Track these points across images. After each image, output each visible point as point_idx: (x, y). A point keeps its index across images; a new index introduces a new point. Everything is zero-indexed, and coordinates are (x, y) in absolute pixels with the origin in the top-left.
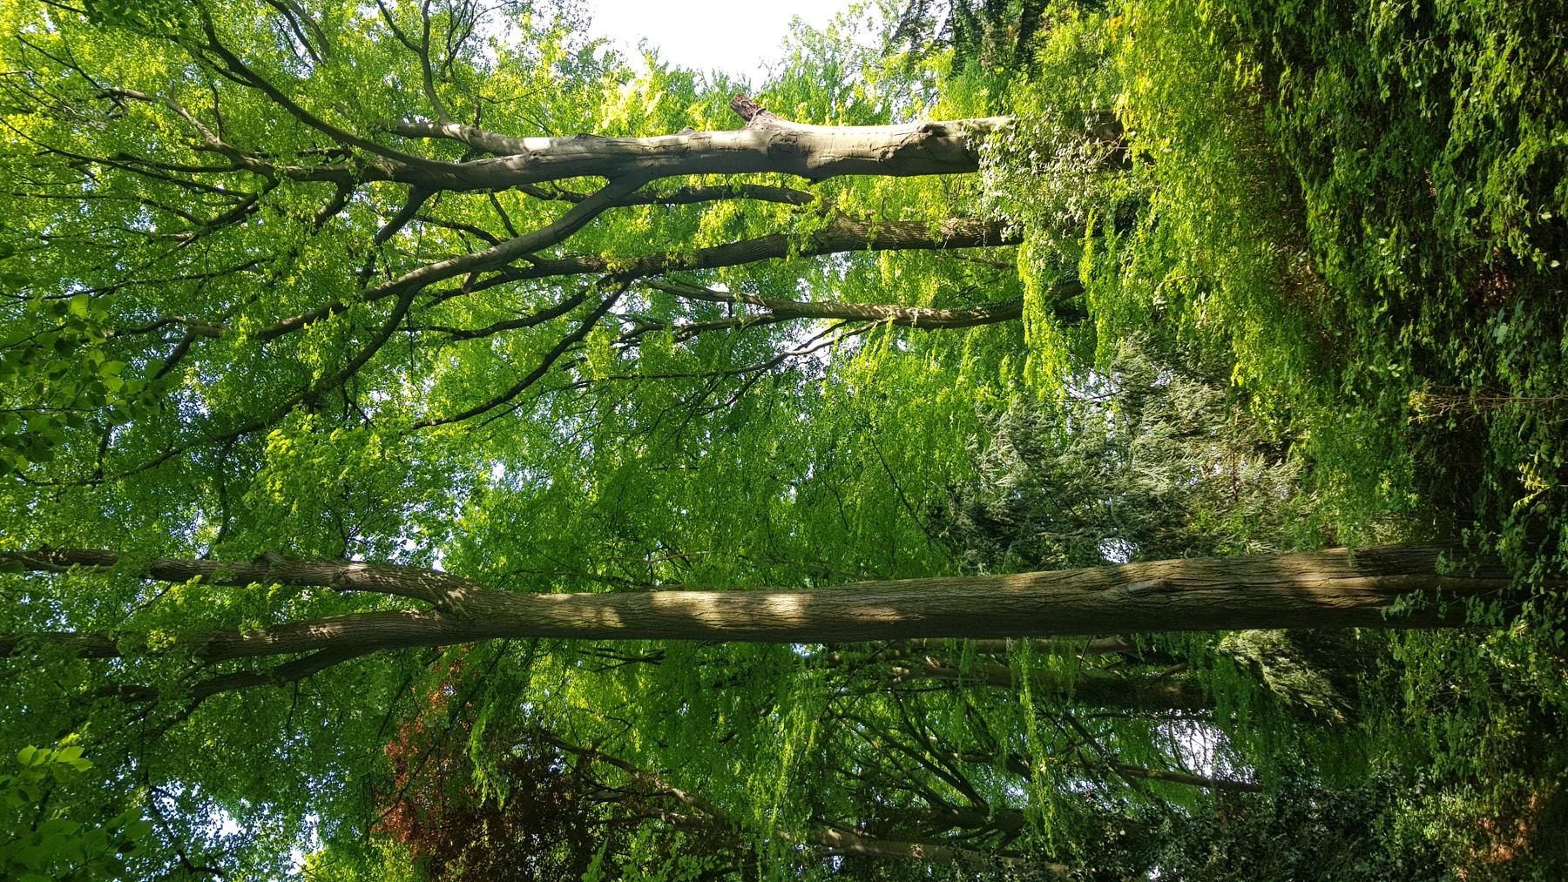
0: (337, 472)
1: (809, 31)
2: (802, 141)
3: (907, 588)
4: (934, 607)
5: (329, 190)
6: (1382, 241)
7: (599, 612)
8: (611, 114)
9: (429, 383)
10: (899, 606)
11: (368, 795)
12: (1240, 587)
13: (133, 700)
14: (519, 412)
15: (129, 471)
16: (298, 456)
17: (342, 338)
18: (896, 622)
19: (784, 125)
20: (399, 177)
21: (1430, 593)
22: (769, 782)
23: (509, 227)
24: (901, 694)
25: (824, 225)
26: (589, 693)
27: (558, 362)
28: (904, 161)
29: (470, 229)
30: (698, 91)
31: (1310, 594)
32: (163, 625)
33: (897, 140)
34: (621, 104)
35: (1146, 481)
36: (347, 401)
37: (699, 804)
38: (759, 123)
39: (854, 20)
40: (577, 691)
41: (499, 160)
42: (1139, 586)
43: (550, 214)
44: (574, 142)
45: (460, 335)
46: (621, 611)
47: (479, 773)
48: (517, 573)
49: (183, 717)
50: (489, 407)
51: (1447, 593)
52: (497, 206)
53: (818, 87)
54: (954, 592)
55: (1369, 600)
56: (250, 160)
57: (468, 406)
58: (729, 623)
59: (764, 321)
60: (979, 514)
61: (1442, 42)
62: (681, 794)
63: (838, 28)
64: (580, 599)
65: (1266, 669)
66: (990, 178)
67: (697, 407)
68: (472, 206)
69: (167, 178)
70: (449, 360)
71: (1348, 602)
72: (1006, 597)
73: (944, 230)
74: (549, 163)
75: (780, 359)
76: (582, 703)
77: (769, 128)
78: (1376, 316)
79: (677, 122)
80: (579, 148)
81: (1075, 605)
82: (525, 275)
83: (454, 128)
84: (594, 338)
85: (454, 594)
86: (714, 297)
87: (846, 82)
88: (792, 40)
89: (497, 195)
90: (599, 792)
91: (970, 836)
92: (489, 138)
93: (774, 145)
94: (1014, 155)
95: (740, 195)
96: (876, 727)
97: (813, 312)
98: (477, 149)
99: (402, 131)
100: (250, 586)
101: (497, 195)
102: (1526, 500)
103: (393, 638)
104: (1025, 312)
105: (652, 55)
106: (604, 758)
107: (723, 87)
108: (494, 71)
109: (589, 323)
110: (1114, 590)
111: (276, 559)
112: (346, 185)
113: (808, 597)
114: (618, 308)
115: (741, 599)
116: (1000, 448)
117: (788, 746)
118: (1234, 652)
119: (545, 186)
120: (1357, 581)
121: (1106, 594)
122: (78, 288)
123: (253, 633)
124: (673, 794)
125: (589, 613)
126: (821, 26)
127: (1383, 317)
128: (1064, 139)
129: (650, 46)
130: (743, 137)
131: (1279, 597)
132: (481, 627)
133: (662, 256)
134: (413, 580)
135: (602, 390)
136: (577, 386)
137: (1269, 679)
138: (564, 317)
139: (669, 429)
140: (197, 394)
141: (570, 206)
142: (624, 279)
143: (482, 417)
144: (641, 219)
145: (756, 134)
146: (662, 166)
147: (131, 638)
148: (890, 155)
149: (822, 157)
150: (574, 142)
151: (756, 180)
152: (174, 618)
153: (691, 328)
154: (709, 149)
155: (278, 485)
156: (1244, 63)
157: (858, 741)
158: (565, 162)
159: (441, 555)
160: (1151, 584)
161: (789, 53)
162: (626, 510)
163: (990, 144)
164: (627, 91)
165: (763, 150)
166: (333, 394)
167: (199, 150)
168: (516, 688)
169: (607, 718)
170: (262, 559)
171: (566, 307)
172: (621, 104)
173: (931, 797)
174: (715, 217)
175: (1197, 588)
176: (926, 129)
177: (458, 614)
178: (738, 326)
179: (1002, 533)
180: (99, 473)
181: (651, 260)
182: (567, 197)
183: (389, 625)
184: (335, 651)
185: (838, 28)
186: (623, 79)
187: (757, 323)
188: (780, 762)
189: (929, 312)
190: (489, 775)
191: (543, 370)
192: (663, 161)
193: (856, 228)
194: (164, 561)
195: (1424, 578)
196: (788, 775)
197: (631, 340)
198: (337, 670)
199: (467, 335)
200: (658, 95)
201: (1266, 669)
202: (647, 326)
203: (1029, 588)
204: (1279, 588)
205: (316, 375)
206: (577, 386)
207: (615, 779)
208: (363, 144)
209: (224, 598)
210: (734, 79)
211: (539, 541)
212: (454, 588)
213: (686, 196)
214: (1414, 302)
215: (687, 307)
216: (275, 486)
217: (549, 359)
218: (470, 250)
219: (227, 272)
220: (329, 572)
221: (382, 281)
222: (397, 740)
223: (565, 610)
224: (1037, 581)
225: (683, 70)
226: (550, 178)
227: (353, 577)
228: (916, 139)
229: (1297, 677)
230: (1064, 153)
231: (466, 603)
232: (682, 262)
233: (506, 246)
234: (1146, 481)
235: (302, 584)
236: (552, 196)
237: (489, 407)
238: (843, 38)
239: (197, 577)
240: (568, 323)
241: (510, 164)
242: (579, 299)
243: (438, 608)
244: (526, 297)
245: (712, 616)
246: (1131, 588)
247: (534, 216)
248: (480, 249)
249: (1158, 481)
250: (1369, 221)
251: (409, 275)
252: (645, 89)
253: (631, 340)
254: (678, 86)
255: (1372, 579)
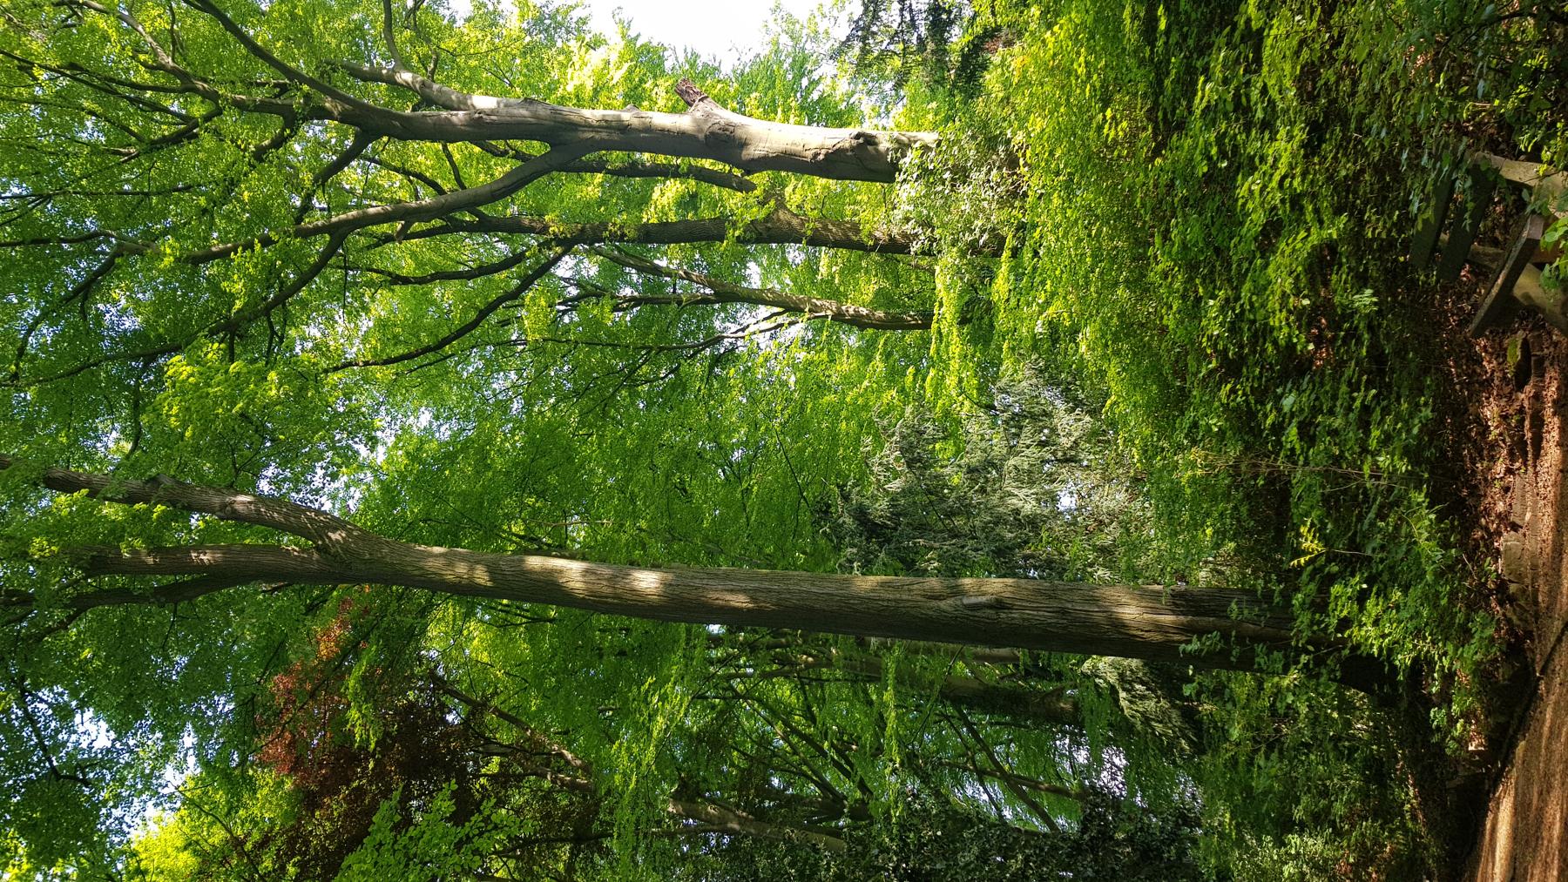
0: (234, 404)
1: (790, 19)
2: (739, 132)
3: (764, 578)
4: (786, 600)
5: (275, 124)
6: (1211, 302)
7: (472, 569)
8: (578, 77)
9: (366, 323)
10: (752, 594)
11: (251, 722)
12: (1063, 612)
13: (14, 604)
14: (450, 363)
15: (44, 376)
16: (197, 384)
17: (271, 272)
18: (749, 610)
19: (726, 116)
20: (344, 119)
21: (1225, 636)
22: (636, 750)
23: (458, 179)
24: (806, 681)
25: (762, 215)
26: (492, 648)
27: (493, 318)
28: (833, 164)
29: (420, 176)
30: (668, 65)
31: (1124, 626)
32: (47, 534)
33: (829, 143)
34: (587, 71)
35: (1015, 501)
36: (274, 333)
37: (586, 769)
38: (700, 110)
39: (835, 13)
40: (478, 640)
41: (444, 114)
42: (973, 600)
43: (502, 168)
44: (520, 105)
45: (397, 280)
46: (492, 571)
47: (354, 714)
48: (425, 521)
49: (64, 626)
50: (422, 355)
51: (1240, 639)
52: (450, 157)
53: (781, 82)
54: (806, 587)
55: (1177, 637)
56: (200, 85)
57: (401, 350)
58: (593, 594)
59: (705, 301)
60: (861, 514)
61: (1247, 128)
62: (569, 756)
63: (818, 19)
64: (455, 554)
65: (1123, 694)
66: (906, 192)
67: (630, 379)
68: (424, 155)
69: (114, 93)
70: (385, 304)
71: (1157, 637)
72: (853, 598)
73: (877, 234)
74: (492, 123)
75: (720, 339)
76: (485, 657)
77: (708, 115)
78: (1204, 371)
79: (635, 97)
80: (524, 112)
81: (913, 612)
82: (471, 228)
83: (406, 77)
84: (533, 299)
85: (335, 536)
86: (657, 271)
87: (815, 76)
88: (771, 25)
89: (450, 147)
90: (489, 748)
91: (859, 828)
92: (440, 91)
93: (712, 133)
94: (932, 172)
95: (686, 175)
96: (777, 712)
97: (755, 299)
98: (428, 101)
99: (356, 73)
100: (137, 506)
101: (450, 147)
102: (1302, 560)
103: (283, 575)
104: (934, 326)
105: (625, 26)
106: (502, 715)
107: (693, 65)
108: (460, 23)
109: (526, 283)
110: (950, 601)
111: (168, 482)
112: (293, 121)
113: (670, 576)
114: (565, 268)
115: (605, 571)
116: (890, 453)
117: (660, 719)
118: (1095, 674)
119: (501, 145)
120: (1168, 619)
121: (942, 604)
122: (16, 190)
123: (134, 552)
124: (561, 755)
125: (462, 569)
126: (802, 15)
127: (1211, 373)
128: (978, 164)
129: (625, 16)
130: (683, 122)
131: (1097, 625)
132: (363, 571)
133: (604, 225)
134: (298, 520)
135: (537, 350)
136: (515, 343)
137: (1124, 703)
138: (504, 274)
139: (597, 398)
140: (122, 310)
141: (520, 163)
142: (567, 245)
143: (413, 364)
144: (592, 187)
145: (695, 120)
146: (602, 140)
147: (13, 544)
148: (821, 157)
149: (755, 151)
150: (520, 105)
151: (707, 163)
152: (56, 529)
153: (633, 299)
154: (649, 129)
155: (175, 410)
156: (1113, 118)
157: (751, 720)
158: (508, 124)
159: (358, 495)
160: (983, 599)
161: (768, 38)
162: (545, 472)
163: (911, 159)
164: (596, 58)
165: (701, 136)
166: (254, 327)
167: (151, 69)
168: (414, 635)
169: (507, 674)
170: (154, 480)
171: (506, 264)
172: (587, 71)
173: (824, 786)
174: (666, 196)
175: (1025, 608)
176: (858, 136)
177: (335, 556)
178: (679, 303)
179: (880, 535)
180: (15, 376)
181: (593, 228)
182: (518, 155)
183: (268, 559)
184: (214, 578)
185: (818, 19)
186: (594, 45)
187: (698, 302)
188: (649, 732)
189: (864, 311)
190: (364, 716)
191: (474, 324)
192: (604, 135)
193: (795, 222)
194: (58, 472)
195: (1223, 623)
196: (656, 746)
197: (572, 304)
198: (219, 597)
199: (405, 281)
200: (626, 66)
201: (1123, 694)
202: (590, 291)
203: (873, 591)
204: (1099, 617)
205: (238, 304)
206: (515, 343)
207: (505, 736)
208: (311, 82)
209: (111, 511)
210: (705, 58)
211: (442, 496)
212: (335, 530)
213: (633, 170)
214: (1241, 359)
215: (635, 277)
216: (172, 410)
217: (483, 314)
218: (417, 198)
219: (164, 192)
220: (217, 500)
221: (316, 219)
222: (288, 672)
223: (439, 563)
224: (883, 584)
225: (655, 44)
226: (506, 138)
227: (239, 508)
228: (847, 145)
229: (1151, 705)
230: (977, 176)
231: (345, 546)
232: (623, 235)
233: (449, 197)
234: (1015, 501)
235: (191, 508)
236: (504, 154)
237: (422, 355)
238: (821, 30)
239: (84, 491)
240: (507, 279)
241: (454, 119)
242: (517, 259)
243: (318, 548)
244: (469, 250)
245: (578, 585)
246: (966, 601)
247: (483, 170)
248: (427, 198)
249: (1025, 501)
250: (1203, 282)
251: (343, 217)
252: (614, 58)
253: (572, 304)
254: (647, 59)
255: (1182, 618)
